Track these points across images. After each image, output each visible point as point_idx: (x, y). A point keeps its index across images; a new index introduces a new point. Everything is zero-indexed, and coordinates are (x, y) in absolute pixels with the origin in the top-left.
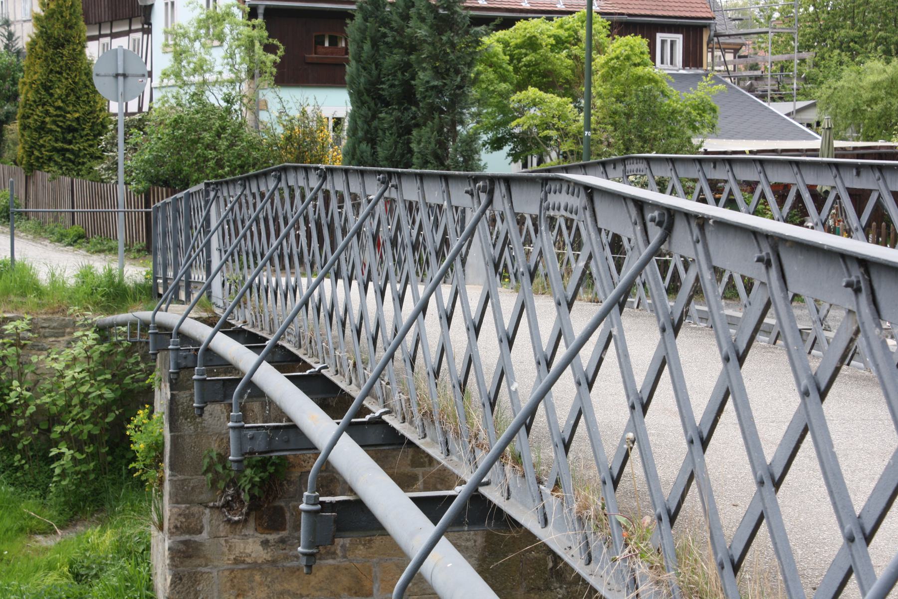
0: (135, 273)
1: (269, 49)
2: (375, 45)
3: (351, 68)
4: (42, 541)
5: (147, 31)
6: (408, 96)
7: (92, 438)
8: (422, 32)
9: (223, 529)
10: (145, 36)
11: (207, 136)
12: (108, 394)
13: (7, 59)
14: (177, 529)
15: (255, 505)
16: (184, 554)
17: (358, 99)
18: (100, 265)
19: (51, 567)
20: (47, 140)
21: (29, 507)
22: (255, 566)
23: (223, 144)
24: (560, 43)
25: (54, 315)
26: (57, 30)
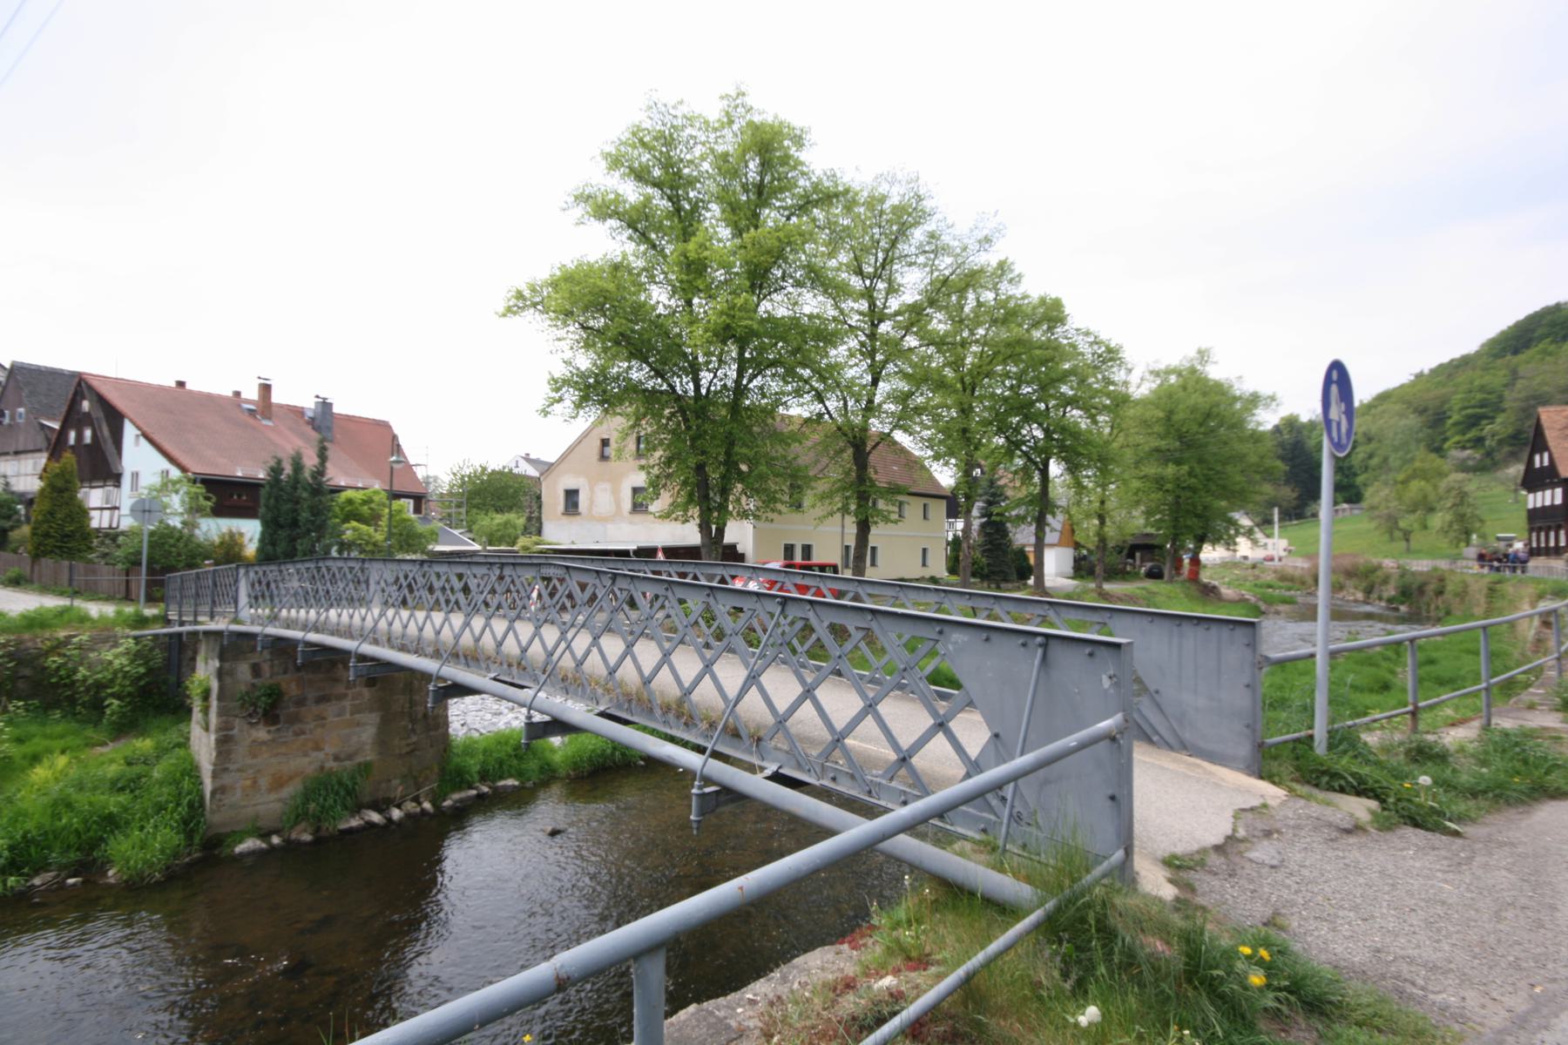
0: (149, 612)
1: (208, 499)
2: (277, 500)
3: (262, 510)
4: (100, 749)
5: (118, 484)
6: (295, 523)
7: (130, 694)
8: (305, 495)
9: (246, 727)
10: (1543, 535)
11: (172, 541)
12: (142, 670)
13: (6, 497)
14: (219, 729)
15: (266, 714)
16: (224, 743)
17: (265, 524)
18: (129, 609)
19: (112, 761)
20: (50, 541)
21: (90, 732)
22: (264, 743)
23: (181, 545)
24: (365, 502)
25: (105, 634)
26: (60, 483)
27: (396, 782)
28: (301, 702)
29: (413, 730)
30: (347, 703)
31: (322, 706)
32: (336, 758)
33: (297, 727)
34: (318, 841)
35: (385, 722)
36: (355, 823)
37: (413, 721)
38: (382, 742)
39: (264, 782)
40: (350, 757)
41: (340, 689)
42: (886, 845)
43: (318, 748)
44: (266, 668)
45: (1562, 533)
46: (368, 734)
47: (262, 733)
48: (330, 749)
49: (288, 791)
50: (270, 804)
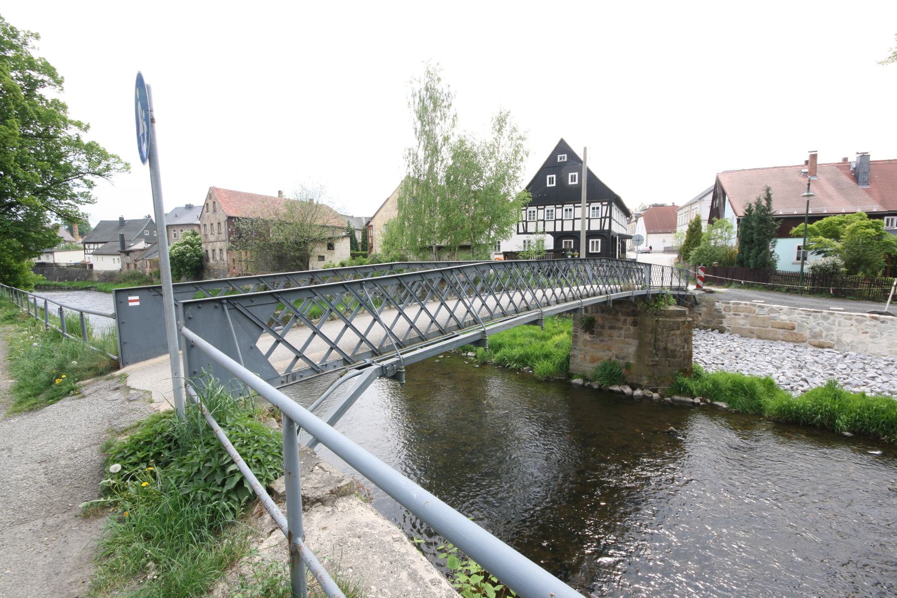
27: (644, 378)
28: (603, 327)
29: (657, 355)
30: (623, 332)
32: (617, 357)
33: (601, 338)
34: (600, 389)
35: (640, 346)
36: (616, 388)
37: (657, 350)
38: (639, 355)
39: (588, 358)
40: (623, 358)
41: (620, 325)
42: (294, 370)
43: (609, 350)
45: (138, 303)
47: (587, 337)
48: (614, 351)
49: (596, 365)
50: (589, 368)
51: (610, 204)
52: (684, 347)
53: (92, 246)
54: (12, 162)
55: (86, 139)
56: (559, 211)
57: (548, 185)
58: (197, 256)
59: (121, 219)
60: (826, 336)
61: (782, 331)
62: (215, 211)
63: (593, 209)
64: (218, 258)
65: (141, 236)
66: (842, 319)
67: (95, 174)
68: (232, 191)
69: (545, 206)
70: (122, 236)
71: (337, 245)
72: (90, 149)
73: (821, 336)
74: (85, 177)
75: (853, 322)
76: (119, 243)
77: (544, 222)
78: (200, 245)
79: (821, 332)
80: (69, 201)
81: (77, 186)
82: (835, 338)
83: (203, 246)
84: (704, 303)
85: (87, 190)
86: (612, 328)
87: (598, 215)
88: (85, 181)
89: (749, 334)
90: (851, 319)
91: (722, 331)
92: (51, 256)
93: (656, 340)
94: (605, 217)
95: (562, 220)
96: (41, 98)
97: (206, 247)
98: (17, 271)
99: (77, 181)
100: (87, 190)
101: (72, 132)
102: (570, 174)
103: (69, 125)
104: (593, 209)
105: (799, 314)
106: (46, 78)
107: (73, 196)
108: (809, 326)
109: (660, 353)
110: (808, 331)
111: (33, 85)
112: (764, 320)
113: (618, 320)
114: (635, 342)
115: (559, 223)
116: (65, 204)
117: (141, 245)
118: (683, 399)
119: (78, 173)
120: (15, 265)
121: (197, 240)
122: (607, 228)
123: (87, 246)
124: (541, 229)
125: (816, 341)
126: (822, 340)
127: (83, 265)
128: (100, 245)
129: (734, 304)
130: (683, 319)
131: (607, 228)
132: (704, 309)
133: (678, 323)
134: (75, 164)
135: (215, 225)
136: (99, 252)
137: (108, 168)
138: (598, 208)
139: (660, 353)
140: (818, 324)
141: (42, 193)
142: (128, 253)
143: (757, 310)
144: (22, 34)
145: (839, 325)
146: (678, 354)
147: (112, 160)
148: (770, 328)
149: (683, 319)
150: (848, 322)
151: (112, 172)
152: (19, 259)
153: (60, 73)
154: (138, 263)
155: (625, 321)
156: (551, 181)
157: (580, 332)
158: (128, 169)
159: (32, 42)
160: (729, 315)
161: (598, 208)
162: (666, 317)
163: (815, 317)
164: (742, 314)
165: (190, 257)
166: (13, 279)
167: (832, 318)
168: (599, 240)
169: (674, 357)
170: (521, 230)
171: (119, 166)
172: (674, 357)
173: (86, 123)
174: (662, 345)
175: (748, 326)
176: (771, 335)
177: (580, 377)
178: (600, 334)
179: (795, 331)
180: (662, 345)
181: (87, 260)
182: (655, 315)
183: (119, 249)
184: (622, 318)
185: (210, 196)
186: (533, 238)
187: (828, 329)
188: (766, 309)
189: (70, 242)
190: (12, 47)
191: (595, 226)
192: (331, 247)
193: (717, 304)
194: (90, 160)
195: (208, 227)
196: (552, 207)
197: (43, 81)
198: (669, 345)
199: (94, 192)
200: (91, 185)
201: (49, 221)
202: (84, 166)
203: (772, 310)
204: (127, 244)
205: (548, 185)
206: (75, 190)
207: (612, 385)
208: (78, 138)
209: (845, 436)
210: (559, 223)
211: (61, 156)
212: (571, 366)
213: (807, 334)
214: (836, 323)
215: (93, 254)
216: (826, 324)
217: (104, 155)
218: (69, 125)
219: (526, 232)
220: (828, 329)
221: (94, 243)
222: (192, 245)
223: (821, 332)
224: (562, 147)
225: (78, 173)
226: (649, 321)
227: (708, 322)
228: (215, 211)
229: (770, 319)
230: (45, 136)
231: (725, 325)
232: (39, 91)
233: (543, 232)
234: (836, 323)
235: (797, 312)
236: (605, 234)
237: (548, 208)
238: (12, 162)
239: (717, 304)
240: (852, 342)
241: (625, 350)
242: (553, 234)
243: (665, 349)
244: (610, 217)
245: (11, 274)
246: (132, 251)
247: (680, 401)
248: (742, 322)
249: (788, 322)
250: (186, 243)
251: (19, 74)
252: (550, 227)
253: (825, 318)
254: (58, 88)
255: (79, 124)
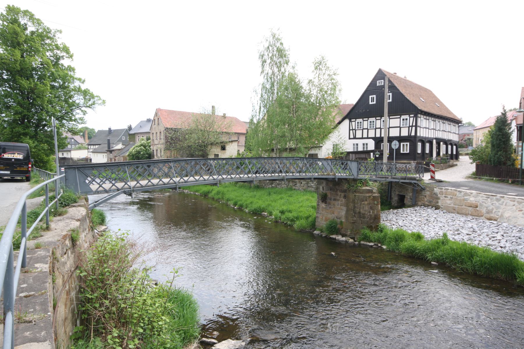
28: (331, 199)
30: (340, 202)
31: (335, 202)
34: (326, 237)
35: (347, 211)
36: (334, 236)
37: (355, 213)
38: (347, 217)
39: (324, 218)
40: (339, 218)
41: (338, 198)
44: (325, 188)
46: (343, 213)
47: (323, 205)
48: (336, 214)
51: (416, 117)
52: (370, 212)
53: (92, 147)
54: (46, 103)
55: (83, 87)
56: (378, 122)
57: (370, 103)
58: (147, 154)
59: (110, 129)
60: (495, 212)
61: (470, 208)
62: (158, 124)
63: (403, 120)
64: (159, 156)
65: (120, 140)
66: (509, 201)
67: (87, 107)
68: (170, 111)
69: (368, 118)
70: (109, 140)
71: (228, 147)
72: (85, 93)
73: (492, 212)
74: (82, 109)
75: (515, 203)
76: (106, 145)
77: (400, 128)
78: (150, 146)
79: (493, 209)
80: (73, 123)
81: (78, 114)
82: (500, 214)
83: (151, 147)
84: (428, 189)
85: (83, 116)
86: (335, 200)
87: (406, 124)
88: (82, 111)
89: (453, 211)
90: (514, 201)
91: (437, 208)
92: (69, 153)
93: (355, 207)
94: (412, 126)
95: (380, 128)
96: (62, 65)
97: (154, 148)
98: (46, 162)
99: (78, 111)
100: (83, 116)
101: (77, 84)
102: (370, 97)
103: (75, 80)
104: (403, 120)
105: (482, 197)
106: (65, 54)
107: (75, 120)
108: (486, 205)
109: (356, 215)
110: (485, 208)
111: (58, 59)
112: (460, 200)
113: (337, 195)
114: (345, 208)
115: (378, 131)
116: (71, 124)
117: (120, 146)
118: (365, 243)
119: (78, 106)
120: (46, 158)
121: (148, 143)
122: (413, 134)
123: (89, 147)
124: (365, 136)
125: (488, 216)
126: (492, 215)
127: (86, 159)
128: (97, 146)
129: (445, 189)
130: (370, 195)
131: (413, 134)
132: (428, 193)
133: (366, 197)
134: (77, 102)
135: (158, 133)
136: (95, 151)
137: (94, 104)
138: (406, 119)
139: (356, 215)
140: (492, 204)
141: (60, 119)
142: (111, 152)
143: (458, 193)
144: (53, 31)
145: (506, 205)
146: (367, 216)
147: (96, 98)
148: (464, 207)
149: (370, 195)
150: (512, 203)
151: (96, 105)
152: (47, 156)
153: (72, 51)
154: (117, 158)
155: (341, 195)
156: (373, 100)
157: (320, 203)
158: (104, 103)
159: (58, 35)
160: (442, 197)
161: (406, 119)
162: (361, 193)
163: (491, 199)
164: (449, 196)
165: (143, 154)
166: (45, 167)
167: (502, 200)
168: (408, 144)
169: (364, 218)
170: (352, 136)
171: (100, 102)
172: (364, 218)
173: (83, 79)
174: (357, 210)
175: (452, 205)
176: (464, 211)
177: (319, 230)
178: (330, 204)
179: (478, 209)
180: (357, 210)
181: (89, 156)
182: (355, 191)
183: (107, 149)
184: (339, 193)
185: (156, 114)
186: (360, 142)
187: (498, 208)
188: (463, 193)
189: (82, 144)
190: (49, 38)
191: (405, 133)
192: (223, 148)
193: (435, 189)
194: (85, 98)
195: (155, 135)
196: (361, 120)
197: (63, 57)
198: (361, 210)
199: (86, 118)
200: (85, 113)
201: (62, 135)
202: (82, 102)
203: (466, 194)
204: (111, 145)
205: (370, 103)
206: (77, 116)
207: (333, 234)
208: (80, 87)
209: (433, 264)
210: (378, 131)
211: (71, 97)
212: (316, 224)
213: (484, 211)
214: (504, 204)
215: (92, 152)
216: (497, 204)
217: (92, 96)
218: (75, 80)
219: (355, 138)
220: (498, 208)
221: (93, 145)
222: (145, 147)
223: (493, 209)
224: (380, 75)
225: (78, 106)
226: (351, 196)
227: (430, 202)
228: (158, 124)
229: (464, 200)
230: (63, 87)
231: (439, 204)
232: (61, 62)
233: (368, 138)
234: (504, 204)
235: (481, 195)
236: (412, 139)
237: (371, 119)
238: (46, 103)
239: (435, 189)
240: (509, 217)
241: (341, 214)
242: (374, 139)
243: (359, 213)
244: (416, 126)
245: (43, 163)
246: (113, 150)
247: (364, 244)
248: (449, 202)
249: (474, 202)
250: (141, 145)
251: (51, 53)
252: (372, 134)
253: (498, 200)
254: (71, 59)
255: (80, 80)
